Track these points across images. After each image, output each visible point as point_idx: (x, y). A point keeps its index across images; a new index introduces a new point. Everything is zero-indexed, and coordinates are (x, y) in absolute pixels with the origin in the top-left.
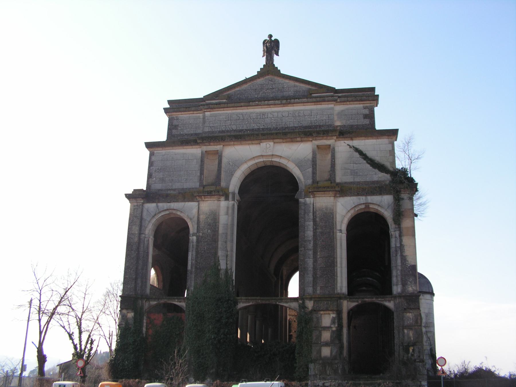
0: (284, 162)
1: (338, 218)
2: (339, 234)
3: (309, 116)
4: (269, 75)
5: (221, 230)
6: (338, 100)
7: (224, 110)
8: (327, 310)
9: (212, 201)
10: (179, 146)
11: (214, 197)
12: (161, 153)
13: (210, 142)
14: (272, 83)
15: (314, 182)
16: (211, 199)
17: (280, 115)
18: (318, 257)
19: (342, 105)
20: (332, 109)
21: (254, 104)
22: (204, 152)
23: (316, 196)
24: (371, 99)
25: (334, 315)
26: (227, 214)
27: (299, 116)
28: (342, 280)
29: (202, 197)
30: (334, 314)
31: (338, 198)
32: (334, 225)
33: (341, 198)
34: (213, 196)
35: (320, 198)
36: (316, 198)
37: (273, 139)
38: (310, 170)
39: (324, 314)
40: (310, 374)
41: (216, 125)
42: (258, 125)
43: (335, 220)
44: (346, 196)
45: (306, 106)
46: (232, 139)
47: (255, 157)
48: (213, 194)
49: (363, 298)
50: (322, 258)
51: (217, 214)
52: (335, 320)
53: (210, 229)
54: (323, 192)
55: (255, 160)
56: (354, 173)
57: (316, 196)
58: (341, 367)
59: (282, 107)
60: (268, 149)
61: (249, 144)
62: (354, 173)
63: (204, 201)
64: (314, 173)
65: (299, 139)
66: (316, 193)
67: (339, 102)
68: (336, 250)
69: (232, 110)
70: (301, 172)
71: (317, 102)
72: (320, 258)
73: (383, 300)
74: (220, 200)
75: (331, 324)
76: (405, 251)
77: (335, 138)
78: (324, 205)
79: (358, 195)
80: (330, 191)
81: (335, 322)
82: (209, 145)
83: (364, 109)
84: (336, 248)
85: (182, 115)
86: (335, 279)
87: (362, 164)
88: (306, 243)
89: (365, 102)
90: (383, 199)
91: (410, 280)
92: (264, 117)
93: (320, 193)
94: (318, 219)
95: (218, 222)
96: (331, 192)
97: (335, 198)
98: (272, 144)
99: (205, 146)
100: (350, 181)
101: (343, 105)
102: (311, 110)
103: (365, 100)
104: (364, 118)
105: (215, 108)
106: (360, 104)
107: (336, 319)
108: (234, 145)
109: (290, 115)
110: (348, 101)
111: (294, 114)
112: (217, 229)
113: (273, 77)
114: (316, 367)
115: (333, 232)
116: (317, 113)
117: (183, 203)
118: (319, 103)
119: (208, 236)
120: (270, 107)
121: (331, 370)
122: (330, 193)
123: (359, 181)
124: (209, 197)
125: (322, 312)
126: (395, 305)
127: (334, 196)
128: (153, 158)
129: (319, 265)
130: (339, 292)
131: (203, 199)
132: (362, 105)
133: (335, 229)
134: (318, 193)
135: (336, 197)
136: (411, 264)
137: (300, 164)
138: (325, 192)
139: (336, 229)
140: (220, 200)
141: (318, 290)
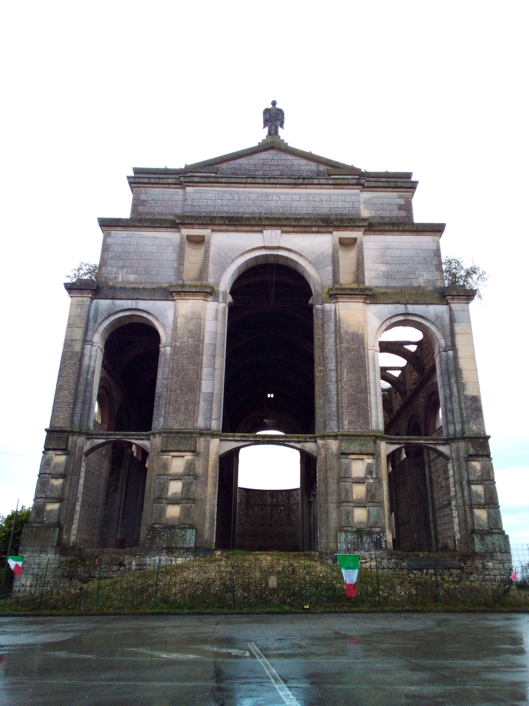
33: (372, 305)
57: (339, 300)
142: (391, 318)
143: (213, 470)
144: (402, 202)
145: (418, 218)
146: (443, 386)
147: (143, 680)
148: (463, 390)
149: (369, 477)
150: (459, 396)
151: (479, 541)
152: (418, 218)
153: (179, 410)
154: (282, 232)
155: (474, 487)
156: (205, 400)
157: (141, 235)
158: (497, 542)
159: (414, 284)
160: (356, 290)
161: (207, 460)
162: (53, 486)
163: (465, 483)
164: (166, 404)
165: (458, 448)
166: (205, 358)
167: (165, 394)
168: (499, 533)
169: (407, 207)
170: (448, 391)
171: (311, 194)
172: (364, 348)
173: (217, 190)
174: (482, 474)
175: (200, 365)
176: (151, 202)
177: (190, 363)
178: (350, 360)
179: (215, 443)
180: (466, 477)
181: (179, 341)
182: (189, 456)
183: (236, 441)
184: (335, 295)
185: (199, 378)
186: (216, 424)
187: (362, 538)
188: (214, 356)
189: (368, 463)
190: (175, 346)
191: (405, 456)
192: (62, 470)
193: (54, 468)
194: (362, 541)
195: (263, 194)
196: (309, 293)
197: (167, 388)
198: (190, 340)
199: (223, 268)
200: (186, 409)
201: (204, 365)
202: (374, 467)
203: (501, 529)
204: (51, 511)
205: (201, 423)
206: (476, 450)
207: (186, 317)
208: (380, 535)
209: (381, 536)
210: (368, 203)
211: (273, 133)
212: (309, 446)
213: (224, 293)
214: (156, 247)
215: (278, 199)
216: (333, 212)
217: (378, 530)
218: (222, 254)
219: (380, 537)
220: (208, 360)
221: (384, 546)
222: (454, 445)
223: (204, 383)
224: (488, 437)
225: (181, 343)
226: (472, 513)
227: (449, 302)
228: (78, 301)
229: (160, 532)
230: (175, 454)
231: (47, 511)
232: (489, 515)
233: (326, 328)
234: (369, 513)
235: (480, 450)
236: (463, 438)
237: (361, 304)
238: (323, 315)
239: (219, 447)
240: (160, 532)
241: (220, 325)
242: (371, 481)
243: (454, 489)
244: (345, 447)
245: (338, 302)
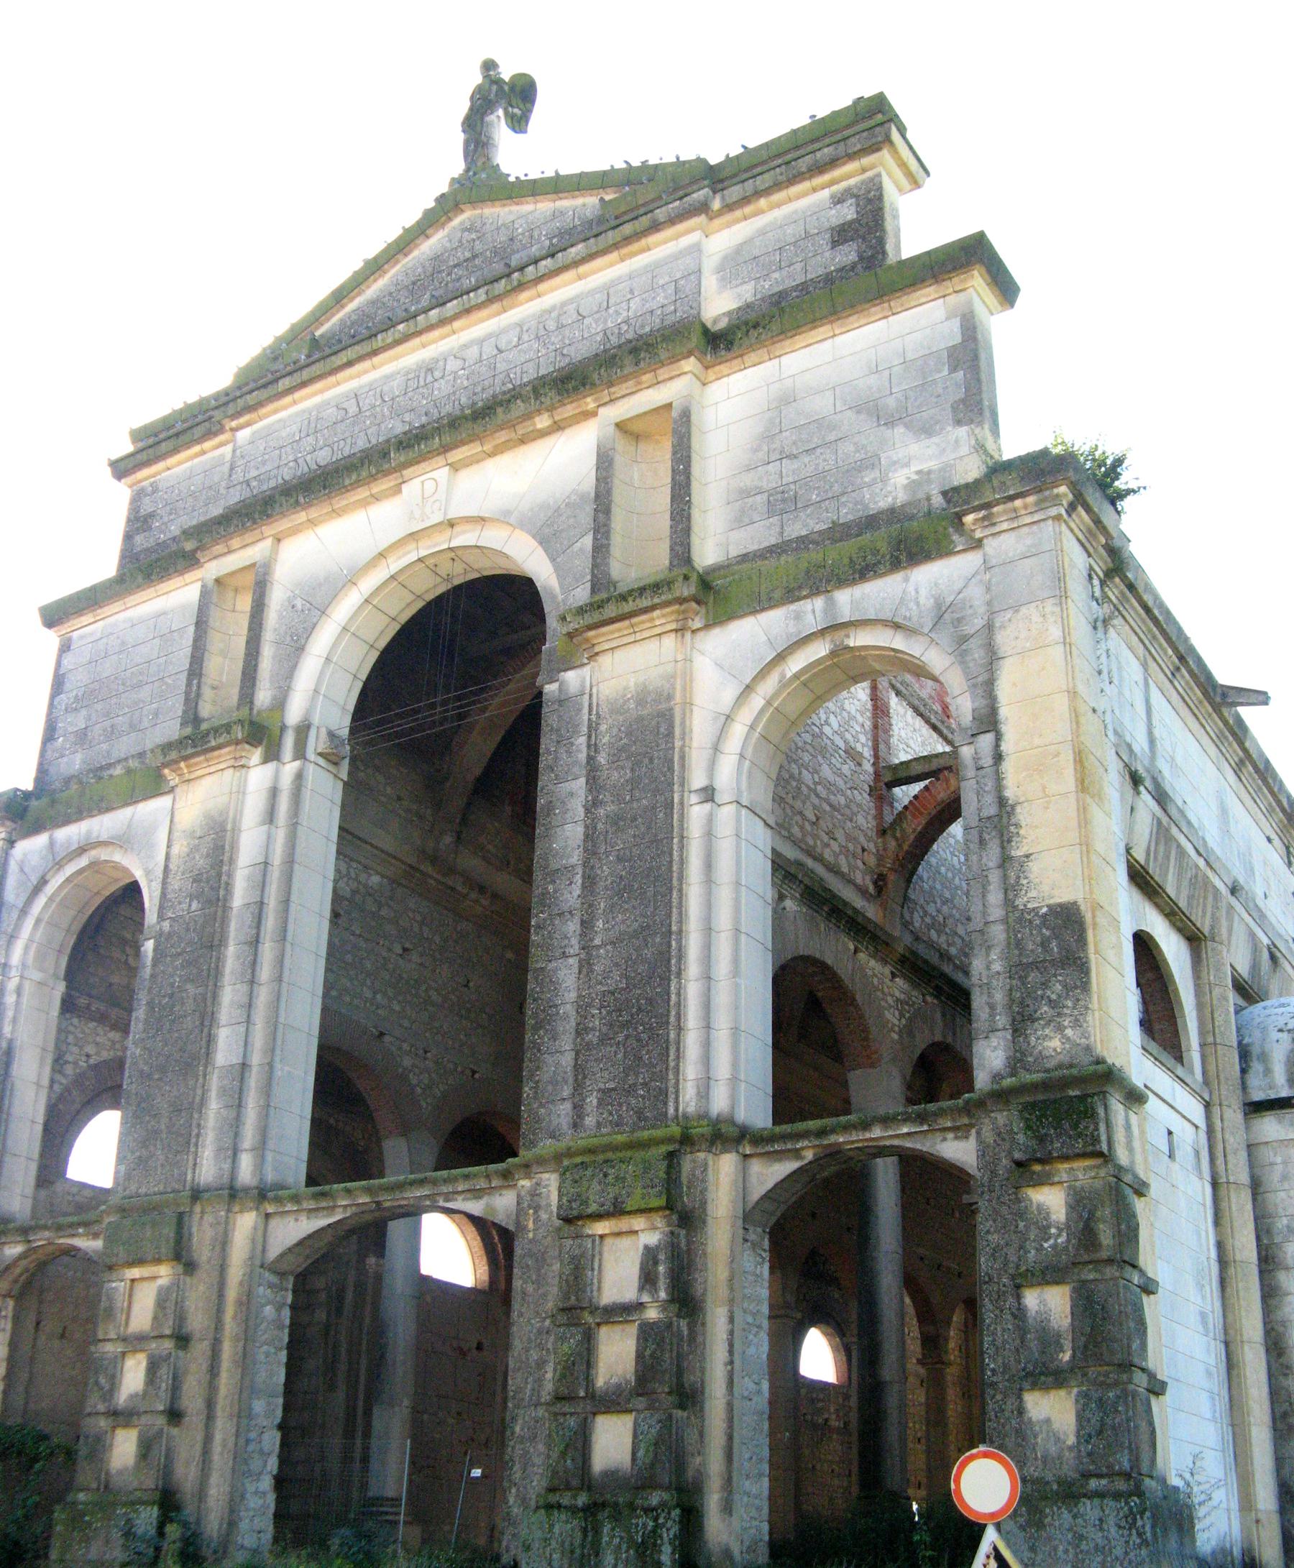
0: (493, 538)
1: (700, 729)
2: (697, 813)
3: (596, 316)
4: (462, 211)
5: (240, 896)
6: (716, 204)
7: (295, 402)
8: (617, 1211)
9: (215, 776)
10: (139, 588)
11: (220, 756)
12: (91, 634)
13: (228, 537)
14: (474, 236)
15: (600, 580)
16: (212, 769)
17: (489, 350)
18: (597, 942)
19: (738, 221)
20: (697, 249)
21: (389, 337)
22: (210, 584)
23: (597, 649)
24: (859, 147)
25: (652, 1238)
26: (270, 816)
27: (560, 327)
28: (707, 1045)
29: (180, 769)
30: (654, 1228)
31: (701, 634)
32: (671, 769)
33: (716, 631)
34: (216, 753)
35: (619, 654)
36: (600, 659)
37: (445, 449)
38: (588, 541)
39: (619, 1234)
40: (156, 1508)
41: (268, 467)
42: (407, 417)
43: (678, 744)
44: (732, 617)
45: (589, 279)
46: (297, 502)
47: (390, 547)
48: (213, 743)
49: (822, 1133)
50: (615, 947)
51: (229, 827)
52: (656, 1263)
53: (197, 898)
54: (626, 623)
55: (1272, 1164)
56: (784, 500)
57: (597, 649)
58: (672, 1533)
59: (499, 314)
60: (432, 500)
61: (364, 503)
62: (784, 500)
63: (188, 781)
64: (601, 549)
65: (542, 422)
66: (596, 637)
67: (720, 213)
68: (680, 890)
69: (322, 391)
70: (553, 560)
71: (628, 240)
72: (604, 944)
73: (925, 1128)
74: (243, 766)
75: (641, 1289)
76: (1022, 832)
77: (690, 364)
78: (632, 684)
79: (791, 595)
80: (653, 608)
81: (657, 1273)
82: (229, 552)
83: (839, 202)
84: (681, 878)
85: (168, 473)
86: (667, 1041)
87: (819, 451)
88: (553, 882)
89: (837, 173)
90: (911, 589)
91: (1049, 993)
92: (430, 379)
93: (612, 632)
94: (602, 759)
95: (232, 861)
96: (657, 613)
97: (683, 636)
98: (442, 474)
99: (215, 558)
100: (766, 544)
101: (745, 218)
102: (607, 289)
103: (833, 163)
104: (835, 244)
105: (260, 404)
106: (814, 190)
107: (662, 1257)
108: (312, 523)
109: (525, 337)
110: (758, 194)
111: (541, 326)
112: (222, 893)
113: (478, 212)
114: (556, 1530)
115: (669, 805)
116: (631, 291)
117: (127, 812)
118: (635, 246)
119: (188, 930)
120: (454, 332)
121: (624, 1547)
122: (652, 620)
123: (804, 533)
124: (200, 762)
125: (601, 1228)
126: (983, 1152)
127: (676, 631)
128: (68, 661)
129: (601, 983)
130: (691, 1109)
131: (187, 777)
132: (826, 193)
133: (676, 787)
134: (603, 634)
135: (688, 635)
136: (1052, 902)
137: (548, 538)
138: (635, 620)
139: (682, 785)
140: (243, 766)
141: (588, 1109)
142: (781, 657)
143: (234, 1318)
151: (1022, 1528)
155: (1032, 1299)
159: (872, 506)
160: (641, 595)
178: (619, 859)
181: (170, 915)
185: (207, 1019)
189: (646, 1247)
202: (662, 1257)
205: (207, 1169)
206: (1042, 1140)
207: (192, 834)
208: (656, 1519)
209: (661, 1521)
212: (502, 1204)
219: (657, 1526)
220: (238, 958)
227: (978, 534)
235: (1059, 1136)
237: (669, 642)
245: (597, 654)
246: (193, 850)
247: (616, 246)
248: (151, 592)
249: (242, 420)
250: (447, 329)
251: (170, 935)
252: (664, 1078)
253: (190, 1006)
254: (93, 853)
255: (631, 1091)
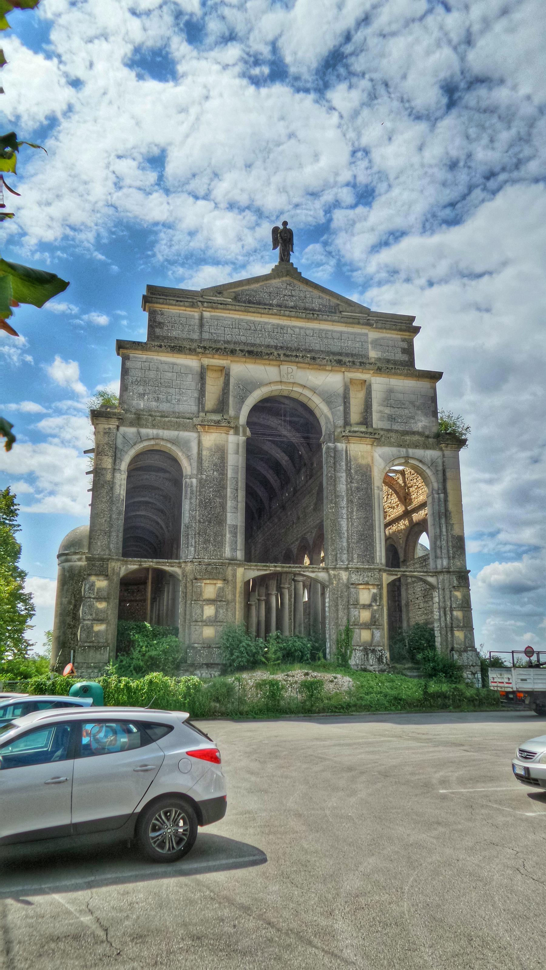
46: (245, 355)
132: (399, 336)
144: (405, 345)
145: (419, 365)
146: (434, 525)
147: (494, 603)
148: (451, 530)
149: (374, 604)
150: (447, 536)
152: (419, 365)
153: (209, 541)
154: (298, 367)
156: (230, 532)
157: (160, 360)
158: (470, 658)
161: (235, 587)
162: (98, 609)
163: (448, 609)
164: (195, 535)
165: (443, 579)
166: (229, 491)
167: (194, 524)
168: (472, 651)
169: (409, 351)
170: (438, 530)
171: (323, 330)
172: (371, 489)
173: (233, 318)
174: (463, 602)
175: (224, 497)
176: (168, 324)
177: (216, 496)
178: (359, 499)
179: (240, 571)
180: (449, 604)
182: (220, 584)
183: (258, 570)
184: (347, 436)
186: (240, 555)
187: (367, 654)
188: (237, 490)
190: (202, 479)
191: (307, 600)
192: (105, 594)
193: (97, 593)
194: (367, 658)
195: (278, 325)
196: (319, 432)
197: (196, 520)
198: (215, 473)
199: (242, 400)
200: (215, 540)
201: (228, 498)
203: (474, 647)
204: (99, 631)
205: (227, 552)
207: (210, 449)
210: (376, 343)
211: (285, 257)
213: (243, 426)
214: (175, 374)
215: (292, 332)
216: (344, 350)
217: (380, 648)
218: (241, 387)
220: (232, 493)
221: (384, 661)
222: (441, 577)
223: (229, 515)
224: (469, 571)
225: (207, 476)
226: (452, 634)
228: (105, 429)
229: (200, 651)
230: (208, 581)
231: (95, 632)
232: (466, 637)
233: (338, 467)
234: (373, 635)
236: (448, 572)
237: (369, 447)
238: (335, 454)
239: (244, 575)
240: (200, 651)
241: (241, 459)
242: (375, 608)
243: (438, 614)
244: (354, 578)
246: (212, 455)
247: (346, 323)
248: (171, 355)
249: (208, 309)
250: (289, 319)
251: (206, 481)
252: (373, 553)
253: (217, 504)
254: (157, 441)
255: (365, 556)
